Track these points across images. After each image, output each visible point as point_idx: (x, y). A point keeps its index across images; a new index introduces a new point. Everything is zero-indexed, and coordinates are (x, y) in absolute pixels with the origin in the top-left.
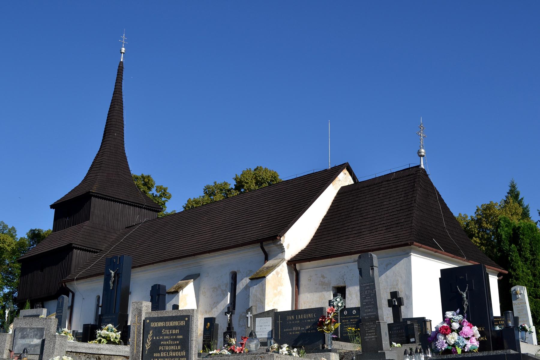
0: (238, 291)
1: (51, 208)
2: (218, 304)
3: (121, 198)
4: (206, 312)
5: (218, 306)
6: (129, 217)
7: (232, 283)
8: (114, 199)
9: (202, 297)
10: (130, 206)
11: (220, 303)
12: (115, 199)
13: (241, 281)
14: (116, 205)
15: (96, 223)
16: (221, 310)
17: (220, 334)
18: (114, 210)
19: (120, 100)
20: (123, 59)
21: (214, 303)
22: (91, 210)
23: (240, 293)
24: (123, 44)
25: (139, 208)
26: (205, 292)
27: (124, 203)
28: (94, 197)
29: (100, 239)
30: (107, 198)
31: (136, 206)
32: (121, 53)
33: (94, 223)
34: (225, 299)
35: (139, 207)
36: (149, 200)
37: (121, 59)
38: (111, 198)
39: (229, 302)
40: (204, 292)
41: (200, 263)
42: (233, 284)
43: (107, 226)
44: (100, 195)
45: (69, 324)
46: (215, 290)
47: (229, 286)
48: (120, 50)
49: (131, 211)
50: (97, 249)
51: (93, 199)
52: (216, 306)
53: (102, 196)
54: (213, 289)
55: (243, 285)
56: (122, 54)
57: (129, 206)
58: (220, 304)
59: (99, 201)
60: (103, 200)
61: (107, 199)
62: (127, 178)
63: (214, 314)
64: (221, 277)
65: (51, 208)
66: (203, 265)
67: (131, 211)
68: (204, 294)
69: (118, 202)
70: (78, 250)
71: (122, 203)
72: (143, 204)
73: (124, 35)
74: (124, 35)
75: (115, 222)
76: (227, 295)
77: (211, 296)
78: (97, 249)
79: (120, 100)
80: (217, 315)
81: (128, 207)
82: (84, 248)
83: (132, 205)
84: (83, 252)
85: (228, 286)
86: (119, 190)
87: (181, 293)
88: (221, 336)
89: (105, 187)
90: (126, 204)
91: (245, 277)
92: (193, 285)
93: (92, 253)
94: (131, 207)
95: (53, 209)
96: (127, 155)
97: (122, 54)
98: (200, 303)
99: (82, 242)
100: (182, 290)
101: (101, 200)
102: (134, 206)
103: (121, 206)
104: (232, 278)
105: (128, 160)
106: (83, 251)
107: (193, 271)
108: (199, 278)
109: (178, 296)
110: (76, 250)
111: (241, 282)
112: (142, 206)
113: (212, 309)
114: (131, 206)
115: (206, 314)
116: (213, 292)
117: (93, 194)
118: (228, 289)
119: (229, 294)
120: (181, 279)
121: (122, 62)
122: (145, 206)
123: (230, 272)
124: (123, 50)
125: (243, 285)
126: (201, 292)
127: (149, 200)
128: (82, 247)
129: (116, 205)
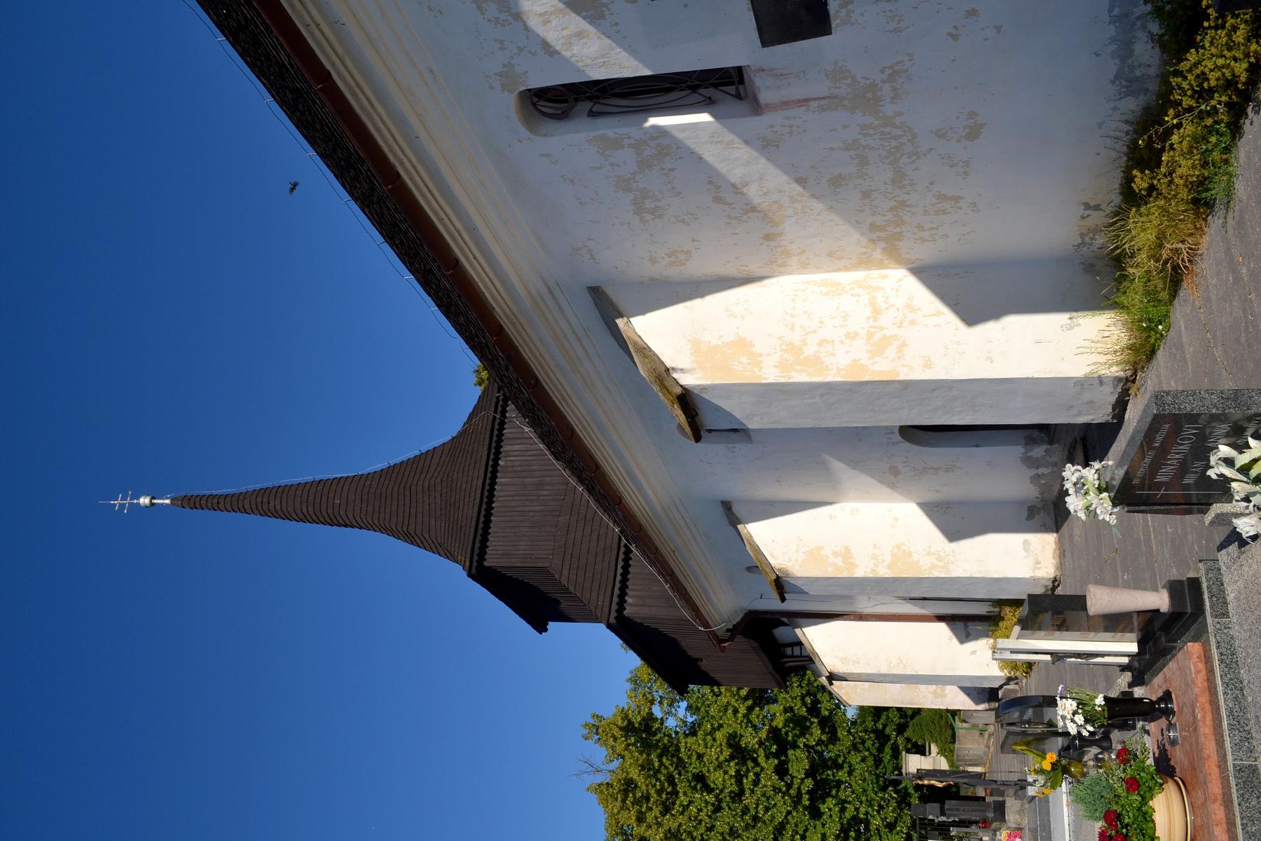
0: (627, 66)
1: (546, 630)
2: (718, 174)
3: (481, 481)
4: (768, 237)
5: (733, 181)
6: (530, 453)
7: (592, 114)
8: (484, 502)
9: (700, 266)
10: (501, 453)
11: (716, 165)
12: (485, 500)
13: (557, 52)
14: (502, 494)
15: (552, 547)
16: (755, 154)
17: (894, 143)
18: (516, 498)
19: (256, 498)
20: (167, 498)
21: (718, 200)
22: (519, 565)
23: (633, 52)
24: (133, 503)
25: (505, 426)
26: (669, 256)
27: (495, 472)
28: (485, 560)
29: (591, 536)
30: (483, 522)
31: (500, 435)
32: (152, 504)
33: (551, 552)
34: (691, 143)
35: (501, 428)
36: (483, 398)
37: (167, 504)
38: (483, 512)
39: (704, 117)
40: (673, 259)
41: (541, 296)
42: (597, 108)
43: (557, 513)
44: (478, 545)
45: (845, 617)
46: (649, 204)
47: (611, 128)
48: (147, 507)
49: (516, 447)
50: (619, 547)
51: (491, 560)
52: (733, 186)
53: (479, 538)
54: (648, 217)
55: (580, 35)
56: (155, 501)
57: (501, 456)
58: (722, 167)
59: (493, 543)
60: (489, 534)
61: (487, 522)
62: (439, 463)
63: (780, 191)
64: (572, 181)
65: (546, 630)
66: (546, 283)
67: (516, 447)
68: (682, 257)
69: (492, 490)
70: (626, 601)
71: (494, 477)
72: (491, 417)
73: (112, 502)
74: (112, 502)
75: (545, 493)
76: (661, 132)
77: (683, 221)
78: (619, 547)
79: (256, 498)
80: (785, 178)
81: (504, 459)
82: (618, 585)
83: (499, 447)
84: (630, 587)
85: (610, 133)
86: (464, 486)
87: (687, 380)
88: (904, 140)
89: (459, 526)
90: (496, 464)
91: (526, 28)
92: (643, 313)
93: (631, 558)
94: (506, 448)
95: (548, 624)
96: (384, 465)
97: (155, 501)
98: (730, 270)
99: (602, 593)
100: (675, 375)
101: (491, 539)
102: (499, 440)
103: (504, 480)
104: (562, 116)
105: (397, 460)
106: (628, 587)
107: (584, 314)
108: (610, 291)
109: (704, 388)
110: (625, 609)
111: (567, 54)
112: (498, 421)
113: (754, 209)
114: (501, 450)
115: (781, 234)
116: (660, 217)
117: (475, 564)
118: (624, 130)
119: (654, 121)
120: (635, 367)
121: (172, 500)
122: (495, 412)
123: (531, 136)
124: (144, 501)
125: (580, 35)
126: (674, 272)
127: (483, 398)
128: (617, 591)
129: (502, 494)
